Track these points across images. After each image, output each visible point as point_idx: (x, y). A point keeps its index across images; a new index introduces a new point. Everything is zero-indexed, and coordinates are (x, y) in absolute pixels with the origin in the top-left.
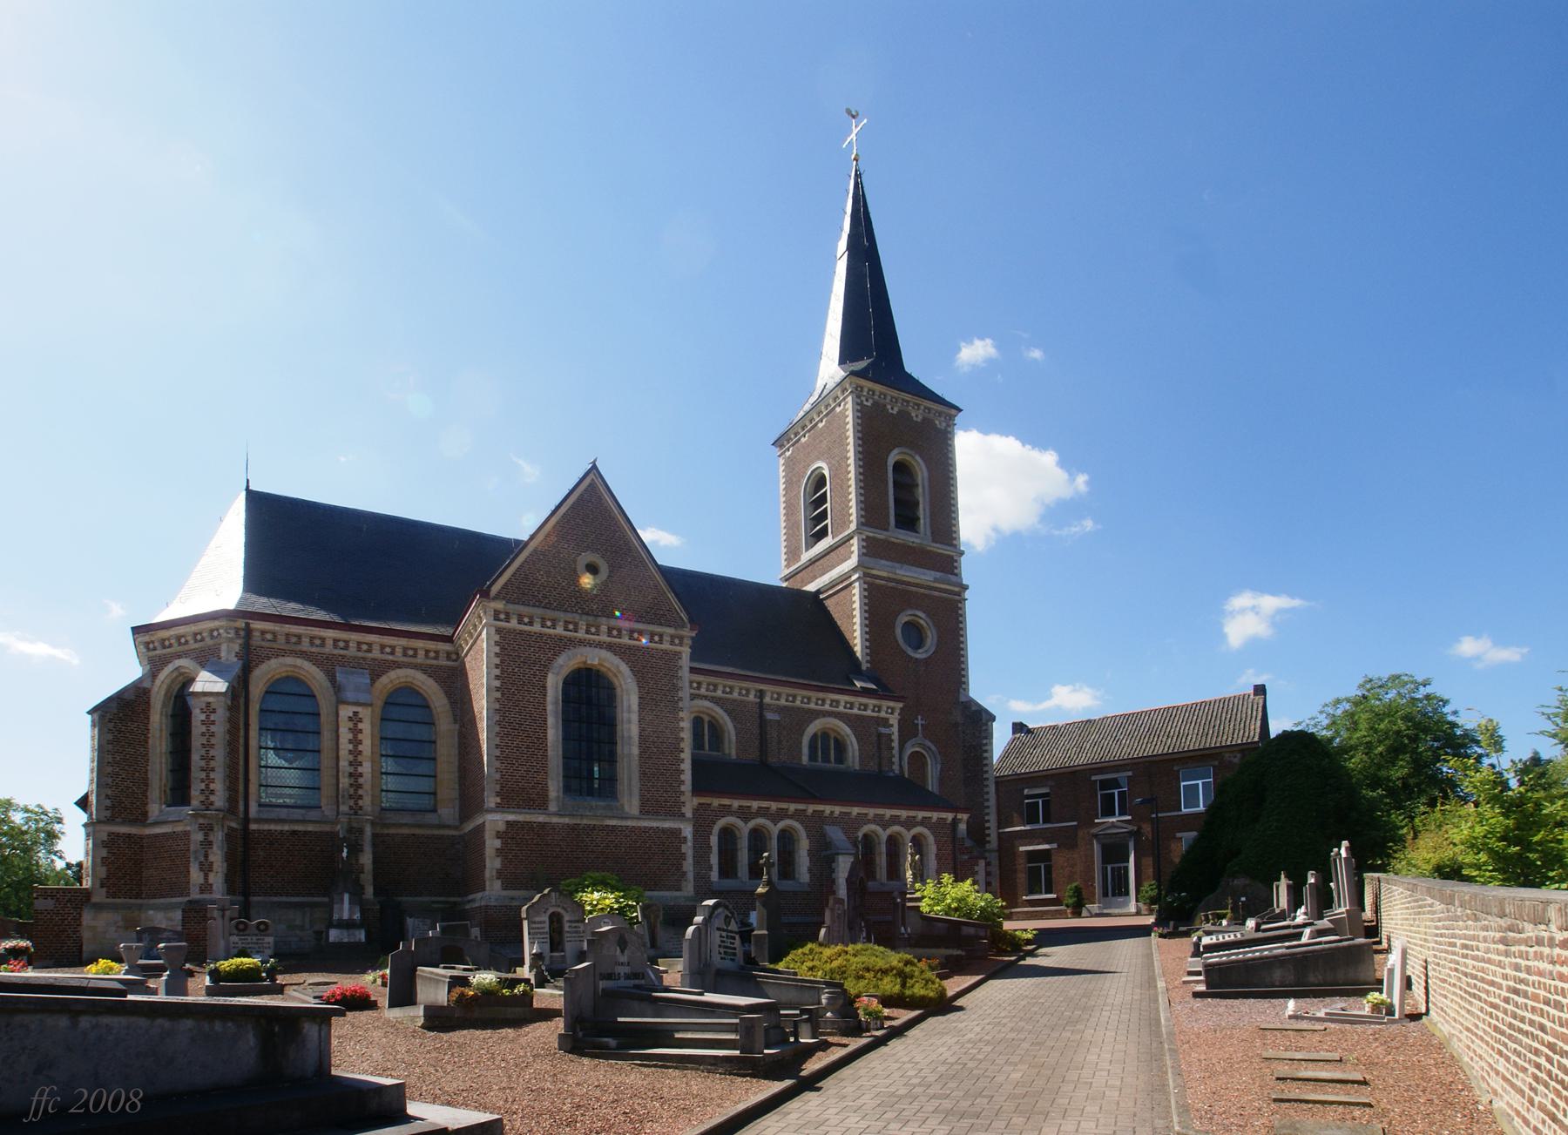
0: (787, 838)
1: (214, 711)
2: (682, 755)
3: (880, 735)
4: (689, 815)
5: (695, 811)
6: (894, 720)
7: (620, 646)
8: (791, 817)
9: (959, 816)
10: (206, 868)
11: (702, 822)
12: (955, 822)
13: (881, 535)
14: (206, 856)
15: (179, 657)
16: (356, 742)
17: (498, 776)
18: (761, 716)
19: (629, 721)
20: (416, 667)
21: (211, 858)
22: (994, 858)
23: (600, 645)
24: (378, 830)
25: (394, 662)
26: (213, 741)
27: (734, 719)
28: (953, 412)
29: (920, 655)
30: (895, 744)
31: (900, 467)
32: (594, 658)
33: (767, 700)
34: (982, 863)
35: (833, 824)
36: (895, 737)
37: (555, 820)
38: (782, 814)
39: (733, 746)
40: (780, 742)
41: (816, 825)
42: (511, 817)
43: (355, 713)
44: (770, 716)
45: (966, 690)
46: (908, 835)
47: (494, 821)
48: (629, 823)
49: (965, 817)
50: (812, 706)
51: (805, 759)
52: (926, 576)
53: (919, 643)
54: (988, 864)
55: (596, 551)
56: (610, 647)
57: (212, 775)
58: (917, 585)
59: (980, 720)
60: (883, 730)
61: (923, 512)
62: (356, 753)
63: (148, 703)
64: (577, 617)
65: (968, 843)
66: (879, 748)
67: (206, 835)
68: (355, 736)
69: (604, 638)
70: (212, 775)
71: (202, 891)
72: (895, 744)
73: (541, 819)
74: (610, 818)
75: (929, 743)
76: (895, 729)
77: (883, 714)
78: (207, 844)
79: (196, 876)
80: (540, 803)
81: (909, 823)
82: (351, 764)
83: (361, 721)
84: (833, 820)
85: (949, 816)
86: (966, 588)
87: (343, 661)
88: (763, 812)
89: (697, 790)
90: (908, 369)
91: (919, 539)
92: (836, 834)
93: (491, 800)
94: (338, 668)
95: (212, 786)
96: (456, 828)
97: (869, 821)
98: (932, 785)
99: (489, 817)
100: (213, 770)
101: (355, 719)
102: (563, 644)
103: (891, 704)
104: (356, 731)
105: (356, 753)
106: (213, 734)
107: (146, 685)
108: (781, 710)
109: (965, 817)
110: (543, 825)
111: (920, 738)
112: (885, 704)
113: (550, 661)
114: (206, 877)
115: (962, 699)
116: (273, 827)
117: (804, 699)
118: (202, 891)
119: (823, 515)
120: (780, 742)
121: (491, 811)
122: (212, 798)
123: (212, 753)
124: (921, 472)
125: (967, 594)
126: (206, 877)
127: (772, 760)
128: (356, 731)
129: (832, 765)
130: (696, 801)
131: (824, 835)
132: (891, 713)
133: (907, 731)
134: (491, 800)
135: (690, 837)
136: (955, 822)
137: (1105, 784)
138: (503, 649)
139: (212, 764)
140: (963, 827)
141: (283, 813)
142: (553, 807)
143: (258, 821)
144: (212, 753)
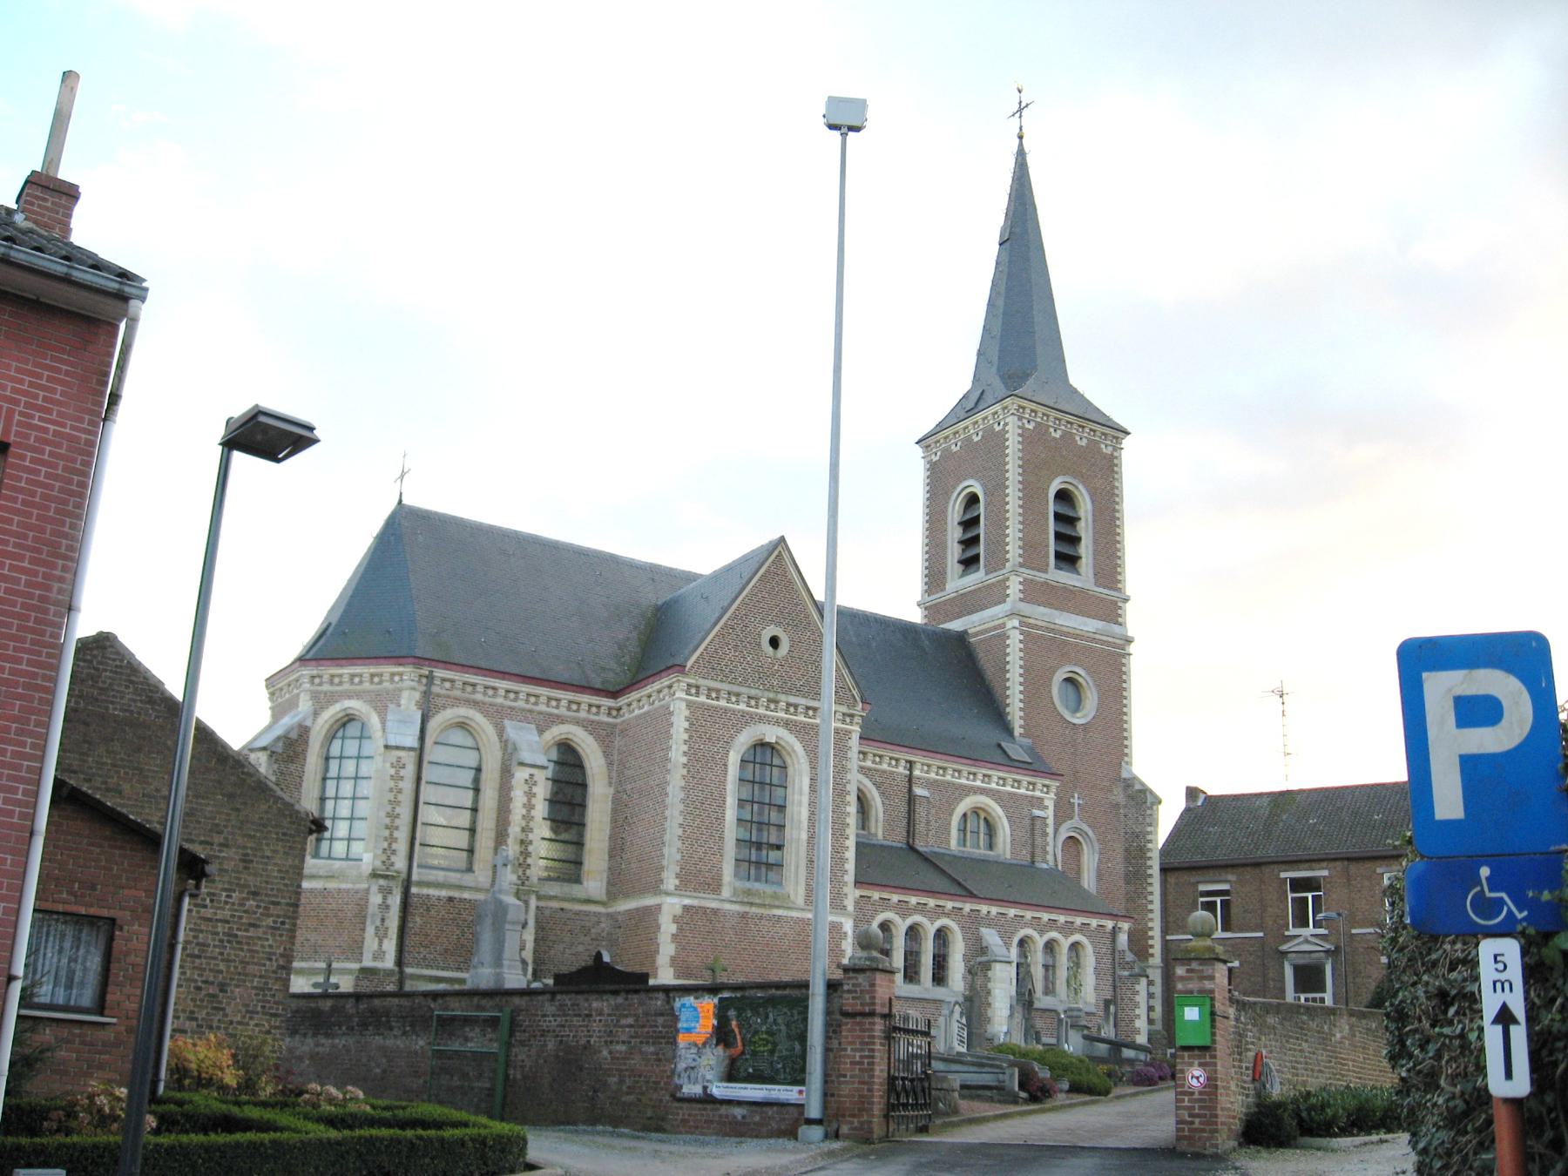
0: (941, 936)
1: (404, 767)
2: (848, 843)
3: (1034, 818)
4: (850, 908)
5: (857, 903)
6: (1049, 802)
7: (796, 723)
8: (948, 915)
9: (1120, 924)
10: (381, 935)
11: (861, 918)
12: (1115, 931)
13: (1040, 577)
14: (383, 920)
15: (350, 697)
16: (529, 807)
17: (679, 857)
18: (910, 790)
19: (800, 804)
20: (578, 722)
21: (387, 923)
22: (1156, 975)
23: (777, 722)
24: (542, 904)
25: (558, 716)
26: (400, 797)
27: (882, 794)
28: (1120, 435)
29: (1078, 720)
30: (1050, 830)
31: (1063, 496)
32: (771, 734)
33: (917, 773)
34: (1144, 981)
35: (989, 926)
36: (1050, 821)
37: (727, 906)
38: (939, 912)
39: (880, 825)
40: (928, 823)
41: (972, 924)
42: (687, 902)
43: (532, 775)
44: (918, 791)
45: (1129, 763)
46: (1065, 943)
47: (671, 905)
48: (795, 914)
49: (1125, 926)
50: (963, 781)
51: (954, 844)
52: (1090, 625)
53: (1078, 706)
54: (1150, 983)
55: (778, 624)
56: (787, 724)
57: (396, 834)
58: (1077, 636)
59: (1142, 800)
60: (1037, 812)
61: (1085, 550)
62: (528, 818)
63: (306, 742)
64: (759, 693)
65: (1129, 957)
66: (1033, 834)
67: (385, 898)
68: (529, 800)
69: (782, 714)
70: (396, 834)
71: (375, 958)
72: (1050, 830)
73: (714, 905)
74: (778, 907)
75: (1085, 827)
76: (1050, 812)
77: (1038, 793)
78: (385, 907)
79: (371, 943)
80: (714, 886)
81: (1068, 929)
82: (523, 830)
83: (535, 784)
84: (989, 922)
85: (1109, 924)
86: (1129, 641)
87: (512, 713)
88: (921, 908)
89: (858, 883)
90: (1074, 380)
91: (1083, 578)
92: (991, 937)
93: (670, 882)
94: (507, 722)
95: (394, 846)
96: (603, 903)
97: (1026, 925)
98: (1088, 881)
99: (670, 900)
100: (397, 828)
101: (531, 782)
102: (747, 719)
103: (1047, 782)
104: (530, 795)
105: (528, 818)
106: (400, 791)
107: (308, 723)
108: (930, 784)
109: (1125, 926)
110: (715, 912)
111: (1075, 821)
112: (1040, 781)
113: (732, 737)
114: (380, 944)
115: (1124, 775)
116: (432, 892)
117: (956, 774)
118: (375, 958)
119: (974, 541)
120: (928, 823)
121: (668, 894)
122: (393, 858)
123: (398, 810)
124: (1085, 507)
125: (1132, 648)
126: (380, 944)
127: (920, 845)
128: (530, 795)
129: (982, 852)
130: (858, 893)
131: (979, 939)
132: (1047, 795)
133: (1063, 811)
134: (670, 882)
135: (850, 933)
136: (1115, 931)
137: (1298, 885)
138: (692, 724)
139: (397, 822)
140: (1123, 939)
141: (440, 876)
142: (726, 892)
143: (420, 884)
144: (398, 810)
